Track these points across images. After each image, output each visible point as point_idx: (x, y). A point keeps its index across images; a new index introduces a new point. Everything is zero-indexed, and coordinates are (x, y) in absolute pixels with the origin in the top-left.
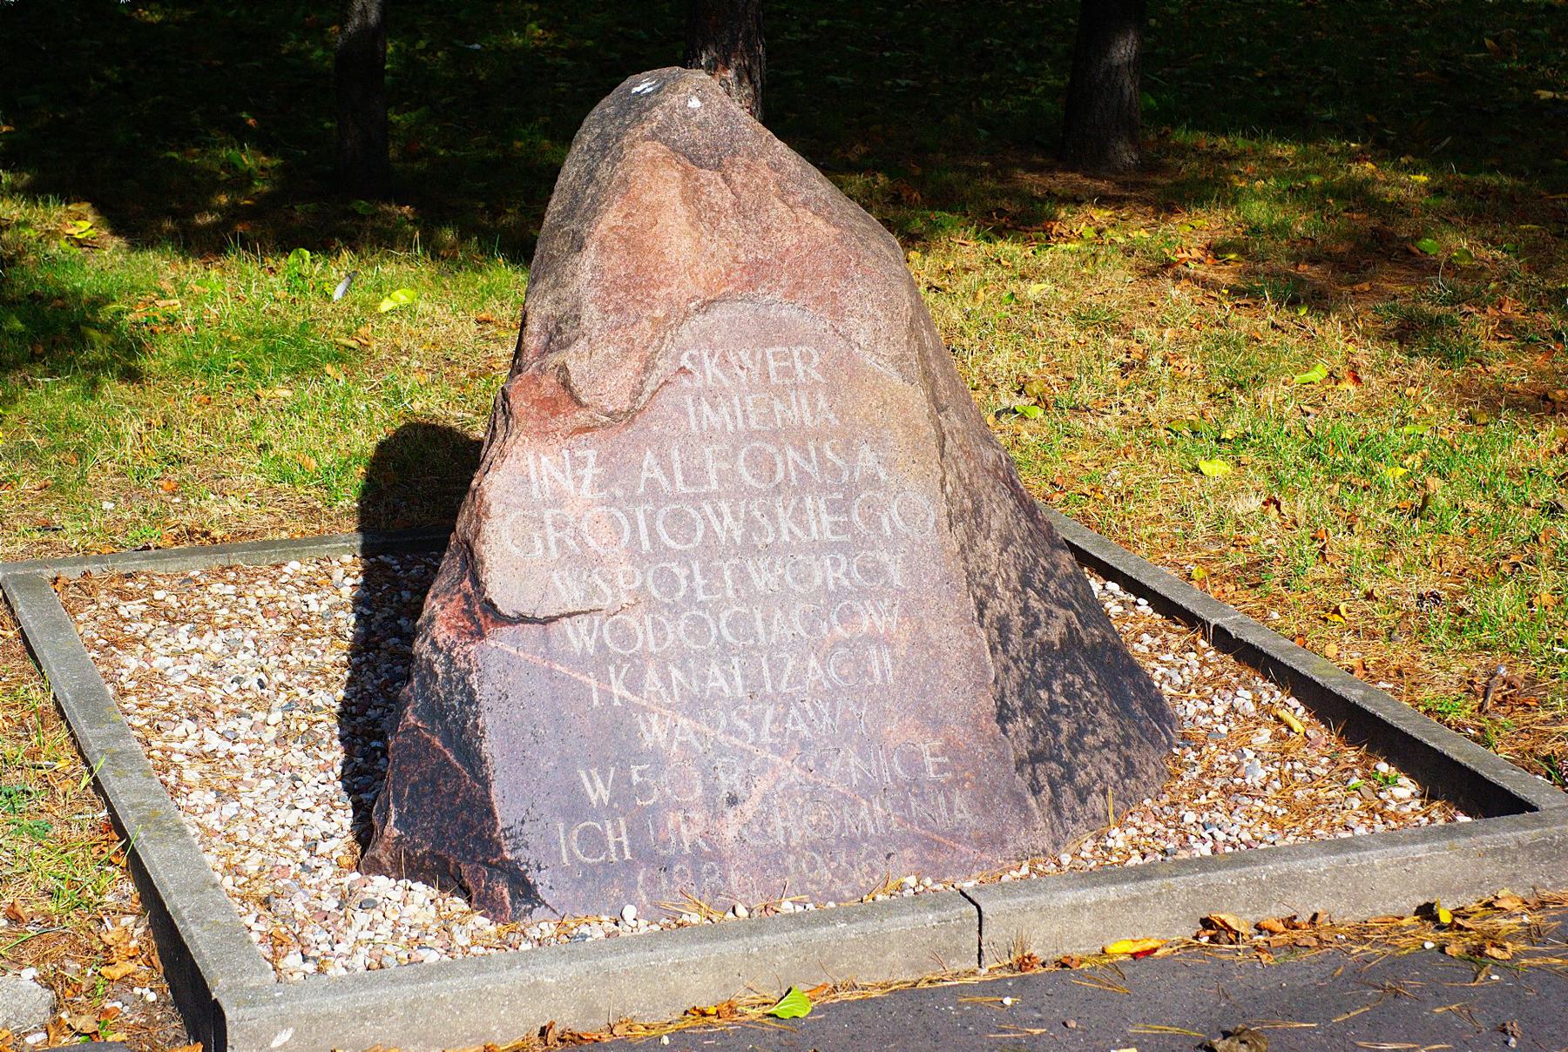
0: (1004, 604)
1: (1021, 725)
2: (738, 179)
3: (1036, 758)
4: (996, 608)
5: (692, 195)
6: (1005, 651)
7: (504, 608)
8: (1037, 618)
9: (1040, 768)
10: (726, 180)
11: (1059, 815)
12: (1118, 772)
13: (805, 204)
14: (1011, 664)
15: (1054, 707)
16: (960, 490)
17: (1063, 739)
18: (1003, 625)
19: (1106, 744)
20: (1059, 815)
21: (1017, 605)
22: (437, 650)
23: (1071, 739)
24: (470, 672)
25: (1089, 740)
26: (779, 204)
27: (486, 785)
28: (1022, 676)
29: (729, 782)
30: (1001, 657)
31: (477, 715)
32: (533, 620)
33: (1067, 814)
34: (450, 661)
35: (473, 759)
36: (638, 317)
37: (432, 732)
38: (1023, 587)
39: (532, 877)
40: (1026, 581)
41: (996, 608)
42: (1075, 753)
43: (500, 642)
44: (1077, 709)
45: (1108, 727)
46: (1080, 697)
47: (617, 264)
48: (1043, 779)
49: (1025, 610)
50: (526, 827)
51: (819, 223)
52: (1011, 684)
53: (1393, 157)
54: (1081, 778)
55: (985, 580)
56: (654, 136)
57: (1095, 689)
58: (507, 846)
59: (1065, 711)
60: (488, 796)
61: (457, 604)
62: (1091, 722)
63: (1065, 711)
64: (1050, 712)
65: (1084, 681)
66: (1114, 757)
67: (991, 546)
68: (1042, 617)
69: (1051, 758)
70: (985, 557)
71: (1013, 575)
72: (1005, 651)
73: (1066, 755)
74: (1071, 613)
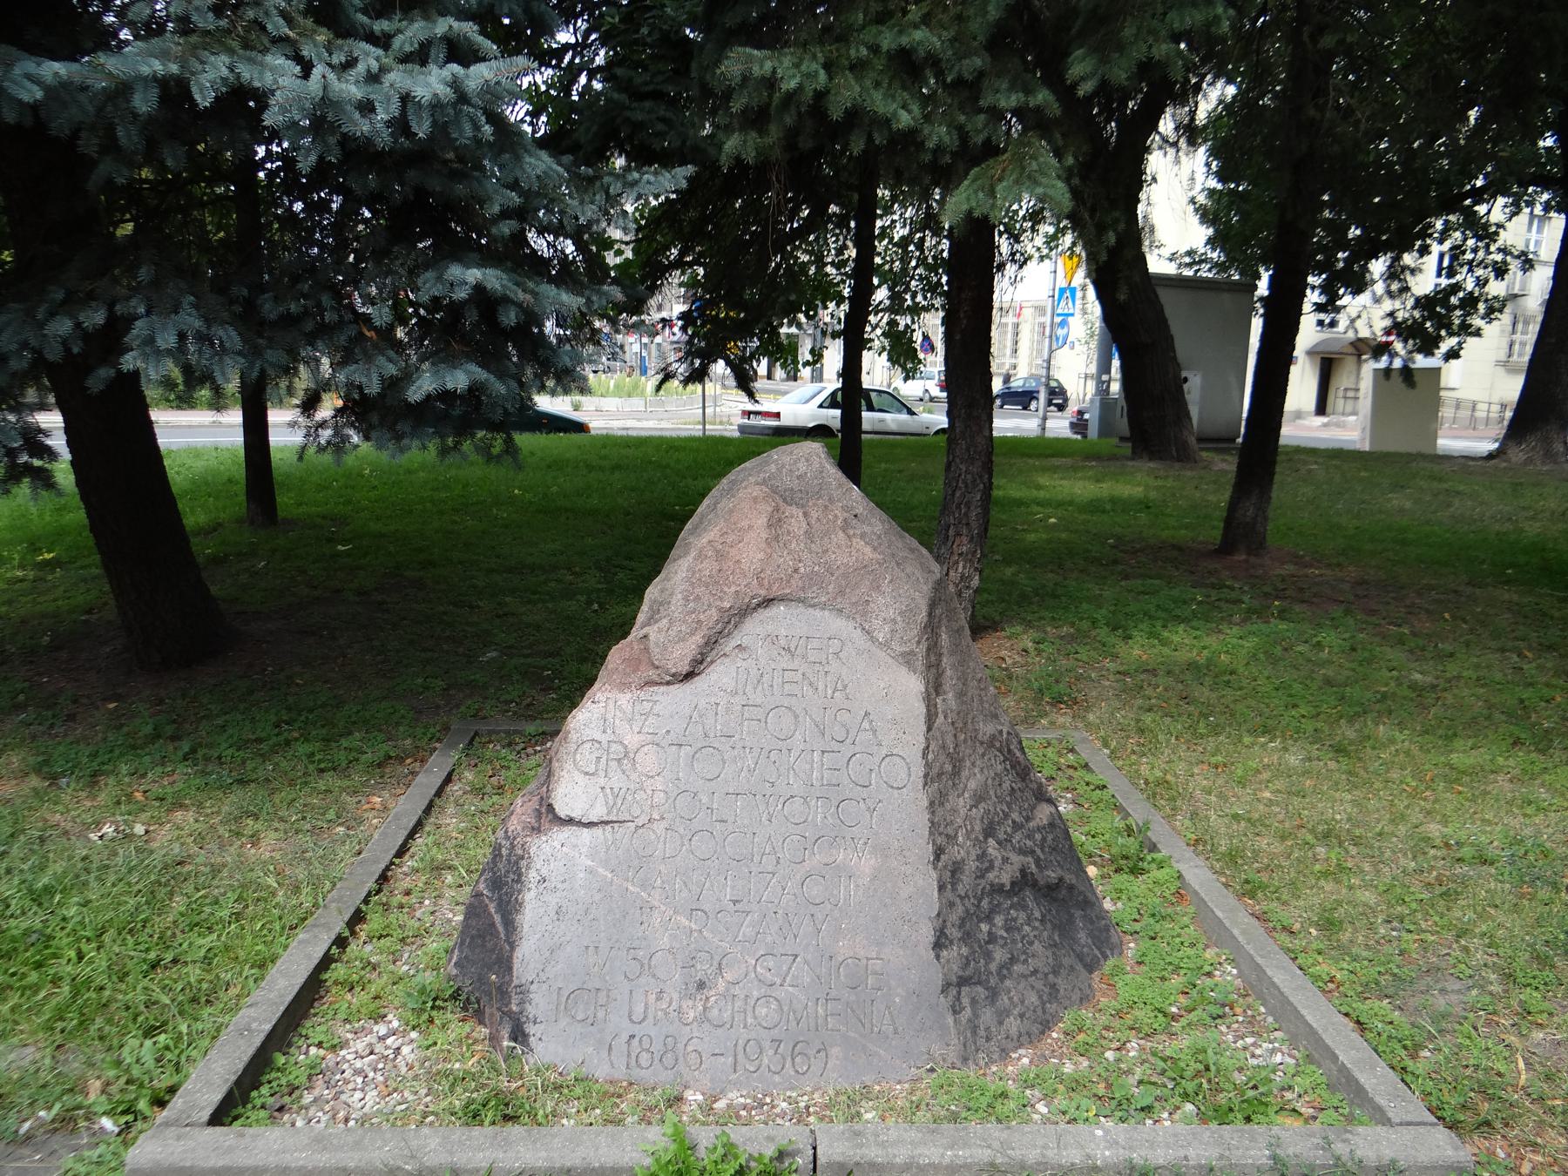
0: (963, 849)
1: (952, 954)
2: (814, 515)
3: (963, 982)
4: (954, 853)
5: (776, 522)
6: (954, 889)
7: (562, 812)
8: (991, 861)
9: (965, 990)
10: (805, 514)
11: (974, 1033)
12: (1040, 997)
13: (863, 536)
14: (958, 900)
15: (992, 939)
16: (942, 758)
17: (993, 967)
18: (956, 869)
19: (1035, 972)
20: (974, 1033)
21: (974, 853)
22: (507, 838)
23: (1001, 967)
24: (522, 858)
25: (1018, 968)
26: (841, 534)
27: (513, 949)
28: (967, 911)
29: (703, 969)
30: (948, 893)
31: (520, 892)
32: (580, 824)
33: (982, 1033)
34: (513, 846)
35: (510, 924)
36: (709, 605)
37: (491, 899)
38: (986, 838)
39: (530, 1029)
40: (989, 832)
41: (954, 853)
42: (1003, 978)
43: (559, 837)
44: (1014, 941)
45: (1041, 956)
46: (1019, 930)
47: (708, 567)
48: (965, 1001)
49: (981, 857)
50: (533, 988)
51: (868, 550)
52: (954, 917)
53: (567, 24)
54: (1004, 1000)
55: (950, 831)
56: (764, 482)
57: (1037, 924)
58: (515, 1000)
59: (1001, 942)
60: (511, 957)
61: (534, 803)
62: (1024, 953)
63: (1001, 942)
64: (988, 943)
65: (1030, 915)
66: (1039, 985)
67: (962, 803)
68: (996, 864)
69: (979, 983)
70: (954, 811)
71: (978, 828)
72: (954, 889)
73: (992, 982)
74: (1030, 859)
